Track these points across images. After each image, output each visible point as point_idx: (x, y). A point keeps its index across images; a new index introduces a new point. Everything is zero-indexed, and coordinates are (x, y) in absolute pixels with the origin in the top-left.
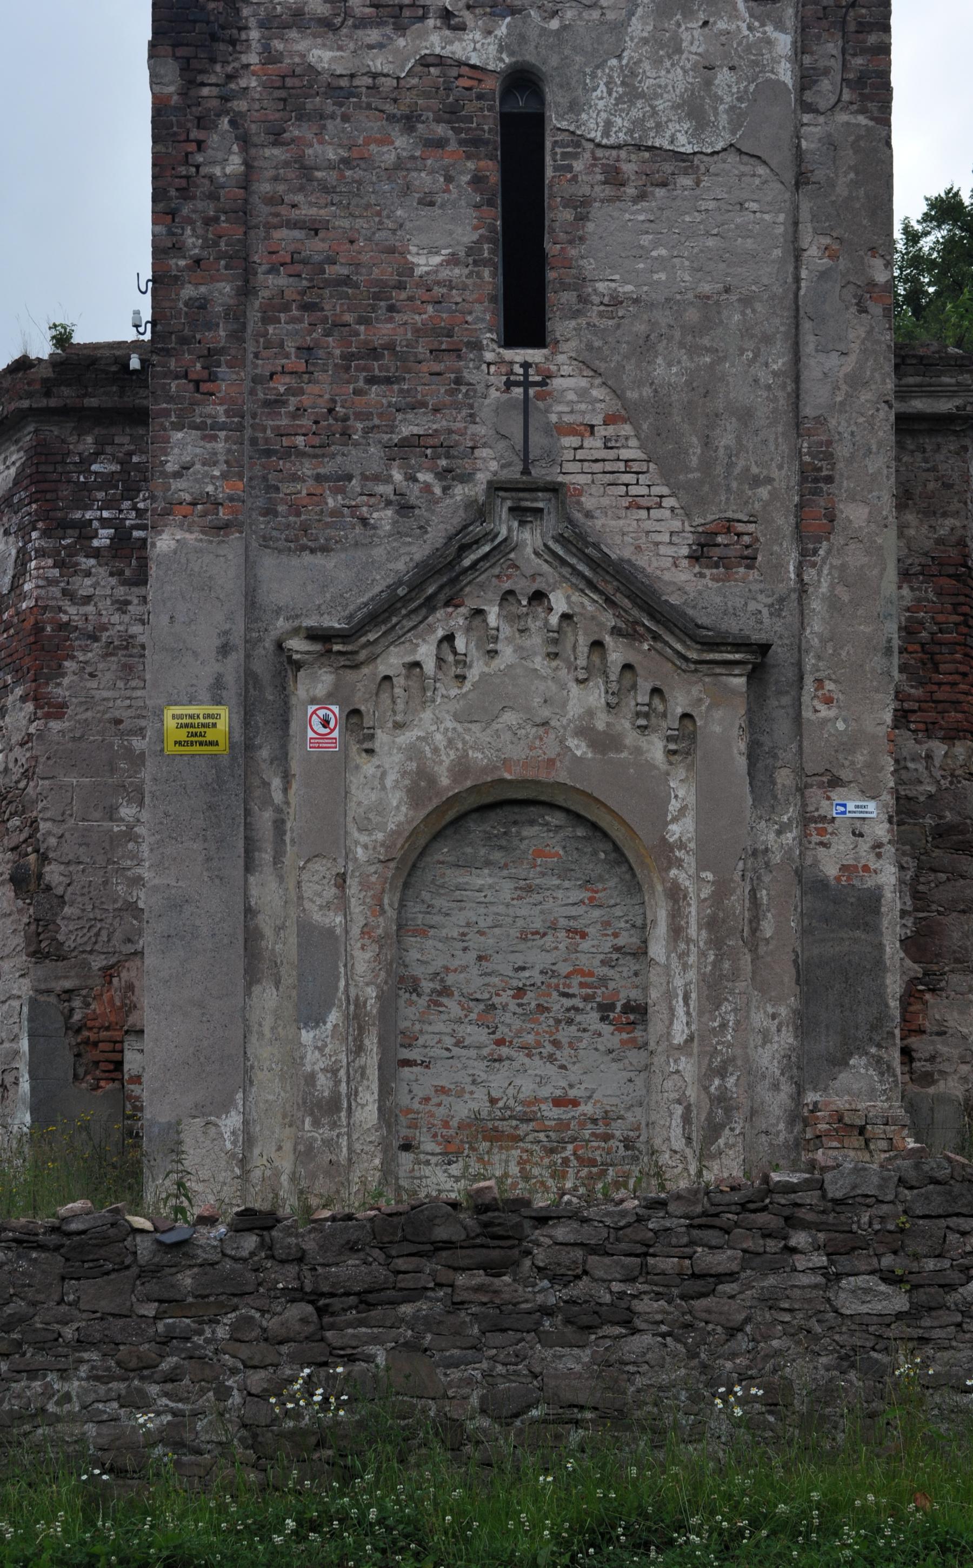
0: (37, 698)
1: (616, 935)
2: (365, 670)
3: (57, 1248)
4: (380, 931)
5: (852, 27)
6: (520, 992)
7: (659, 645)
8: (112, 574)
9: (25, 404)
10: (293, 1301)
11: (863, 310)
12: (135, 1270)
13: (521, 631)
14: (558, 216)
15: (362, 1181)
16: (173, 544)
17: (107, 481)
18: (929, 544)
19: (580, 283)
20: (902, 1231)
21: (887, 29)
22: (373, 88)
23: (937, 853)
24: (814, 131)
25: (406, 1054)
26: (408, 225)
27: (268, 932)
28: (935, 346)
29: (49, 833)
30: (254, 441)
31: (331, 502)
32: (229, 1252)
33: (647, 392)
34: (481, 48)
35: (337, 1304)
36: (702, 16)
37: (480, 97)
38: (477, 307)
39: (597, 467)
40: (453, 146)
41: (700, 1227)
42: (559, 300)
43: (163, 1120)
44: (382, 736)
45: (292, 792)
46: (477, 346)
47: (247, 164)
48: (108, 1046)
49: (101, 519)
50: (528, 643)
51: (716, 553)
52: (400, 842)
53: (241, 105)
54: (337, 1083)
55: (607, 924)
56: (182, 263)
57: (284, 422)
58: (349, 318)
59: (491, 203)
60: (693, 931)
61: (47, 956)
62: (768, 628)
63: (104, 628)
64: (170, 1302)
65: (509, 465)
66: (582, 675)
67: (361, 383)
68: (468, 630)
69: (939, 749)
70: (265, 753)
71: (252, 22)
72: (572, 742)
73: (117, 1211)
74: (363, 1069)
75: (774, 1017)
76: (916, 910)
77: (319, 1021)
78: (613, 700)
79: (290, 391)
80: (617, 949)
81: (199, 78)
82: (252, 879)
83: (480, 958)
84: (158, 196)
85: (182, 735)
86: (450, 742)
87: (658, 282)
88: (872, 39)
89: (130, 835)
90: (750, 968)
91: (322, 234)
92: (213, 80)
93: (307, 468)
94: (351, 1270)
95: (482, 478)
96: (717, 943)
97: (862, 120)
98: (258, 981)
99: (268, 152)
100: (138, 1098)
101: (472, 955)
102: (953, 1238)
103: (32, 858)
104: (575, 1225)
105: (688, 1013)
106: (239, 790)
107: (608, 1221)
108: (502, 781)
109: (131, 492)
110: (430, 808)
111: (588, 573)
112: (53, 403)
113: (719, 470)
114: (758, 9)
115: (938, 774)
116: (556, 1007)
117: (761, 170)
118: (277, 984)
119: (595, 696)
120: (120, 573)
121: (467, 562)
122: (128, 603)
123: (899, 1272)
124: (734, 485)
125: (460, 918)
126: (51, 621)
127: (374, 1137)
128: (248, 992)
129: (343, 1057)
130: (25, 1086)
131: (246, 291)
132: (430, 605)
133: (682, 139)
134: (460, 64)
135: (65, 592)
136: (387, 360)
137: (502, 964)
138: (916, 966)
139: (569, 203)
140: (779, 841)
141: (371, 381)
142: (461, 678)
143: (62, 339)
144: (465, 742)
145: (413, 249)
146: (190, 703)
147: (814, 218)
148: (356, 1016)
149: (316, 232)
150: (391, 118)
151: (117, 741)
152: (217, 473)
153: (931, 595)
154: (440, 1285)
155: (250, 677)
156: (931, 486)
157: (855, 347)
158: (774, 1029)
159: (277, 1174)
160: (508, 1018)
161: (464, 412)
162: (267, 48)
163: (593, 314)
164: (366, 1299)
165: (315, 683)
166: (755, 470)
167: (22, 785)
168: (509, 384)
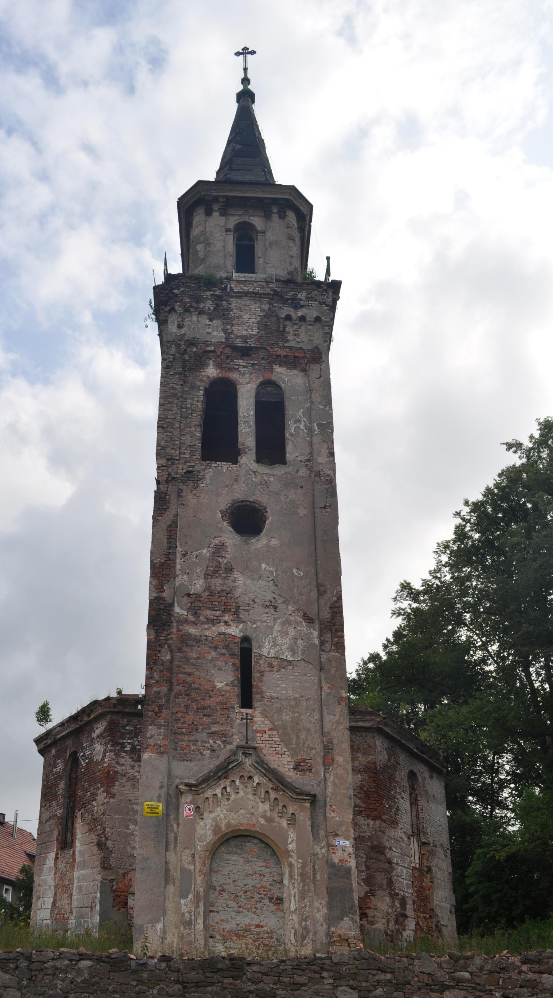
0: (107, 792)
1: (274, 877)
2: (201, 795)
3: (109, 962)
4: (204, 871)
5: (334, 631)
6: (245, 892)
7: (285, 793)
8: (130, 758)
9: (108, 710)
10: (176, 984)
11: (340, 704)
12: (130, 971)
13: (246, 787)
14: (256, 675)
15: (199, 947)
16: (148, 757)
17: (130, 732)
18: (365, 763)
19: (262, 693)
20: (355, 973)
21: (343, 631)
22: (206, 639)
23: (372, 853)
24: (324, 657)
25: (212, 909)
26: (215, 675)
27: (172, 869)
28: (364, 708)
29: (109, 832)
30: (171, 730)
31: (192, 748)
32: (158, 967)
33: (280, 722)
34: (235, 631)
35: (189, 985)
36: (294, 626)
37: (235, 643)
38: (234, 697)
39: (267, 742)
40: (227, 655)
41: (295, 969)
42: (256, 697)
43: (139, 924)
44: (206, 815)
45: (180, 829)
46: (233, 708)
47: (172, 657)
48: (123, 897)
49: (128, 743)
50: (247, 790)
51: (301, 768)
52: (210, 845)
53: (171, 642)
54: (191, 916)
55: (271, 873)
56: (153, 682)
57: (180, 725)
58: (198, 698)
59: (237, 670)
60: (296, 877)
61: (106, 868)
62: (316, 790)
63: (127, 773)
64: (140, 981)
65: (242, 740)
66: (263, 801)
67: (201, 716)
68: (230, 786)
69: (371, 822)
70: (172, 817)
71: (174, 621)
72: (260, 819)
73: (125, 953)
74: (199, 912)
75: (321, 904)
76: (367, 870)
77: (186, 897)
78: (272, 808)
79: (182, 717)
80: (274, 881)
81: (160, 635)
82: (167, 853)
83: (234, 881)
84: (148, 664)
85: (149, 810)
86: (225, 817)
87: (283, 693)
88: (339, 634)
89: (132, 834)
90: (313, 889)
91: (191, 676)
92: (163, 635)
93: (186, 738)
94: (193, 976)
95: (235, 743)
96: (303, 881)
97: (337, 654)
98: (169, 884)
99: (177, 654)
100: (132, 914)
101: (231, 880)
102: (370, 976)
103: (103, 839)
104: (259, 966)
105: (295, 901)
106: (165, 828)
107: (268, 966)
108: (240, 829)
109: (137, 736)
110: (219, 836)
111: (264, 772)
112: (116, 710)
113: (301, 745)
114: (309, 625)
115: (371, 830)
116: (256, 897)
117: (311, 666)
118: (174, 885)
119: (267, 807)
120: (133, 758)
121: (230, 767)
122: (134, 766)
123: (355, 986)
124: (305, 749)
125: (228, 869)
126: (112, 770)
127: (202, 933)
128: (165, 887)
129: (193, 908)
130: (98, 908)
131: (170, 690)
132: (220, 778)
133: (289, 657)
134: (229, 635)
135: (117, 762)
136: (209, 710)
137: (240, 883)
138: (367, 888)
139: (258, 671)
140: (321, 851)
141: (204, 715)
142: (228, 799)
143: (119, 692)
144: (229, 818)
145: (216, 681)
146: (151, 801)
147: (325, 679)
148: (197, 896)
149: (190, 675)
150: (211, 647)
151: (130, 806)
152: (161, 738)
153: (367, 777)
154: (219, 982)
155: (168, 795)
156: (365, 746)
157: (338, 713)
158: (321, 907)
159: (173, 942)
160: (242, 899)
161: (230, 725)
162: (178, 628)
163: (265, 701)
164: (198, 985)
165: (187, 798)
166: (311, 745)
167: (102, 817)
168: (242, 719)
